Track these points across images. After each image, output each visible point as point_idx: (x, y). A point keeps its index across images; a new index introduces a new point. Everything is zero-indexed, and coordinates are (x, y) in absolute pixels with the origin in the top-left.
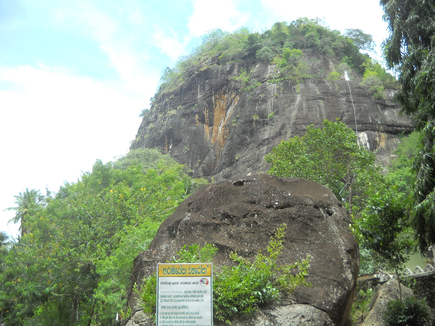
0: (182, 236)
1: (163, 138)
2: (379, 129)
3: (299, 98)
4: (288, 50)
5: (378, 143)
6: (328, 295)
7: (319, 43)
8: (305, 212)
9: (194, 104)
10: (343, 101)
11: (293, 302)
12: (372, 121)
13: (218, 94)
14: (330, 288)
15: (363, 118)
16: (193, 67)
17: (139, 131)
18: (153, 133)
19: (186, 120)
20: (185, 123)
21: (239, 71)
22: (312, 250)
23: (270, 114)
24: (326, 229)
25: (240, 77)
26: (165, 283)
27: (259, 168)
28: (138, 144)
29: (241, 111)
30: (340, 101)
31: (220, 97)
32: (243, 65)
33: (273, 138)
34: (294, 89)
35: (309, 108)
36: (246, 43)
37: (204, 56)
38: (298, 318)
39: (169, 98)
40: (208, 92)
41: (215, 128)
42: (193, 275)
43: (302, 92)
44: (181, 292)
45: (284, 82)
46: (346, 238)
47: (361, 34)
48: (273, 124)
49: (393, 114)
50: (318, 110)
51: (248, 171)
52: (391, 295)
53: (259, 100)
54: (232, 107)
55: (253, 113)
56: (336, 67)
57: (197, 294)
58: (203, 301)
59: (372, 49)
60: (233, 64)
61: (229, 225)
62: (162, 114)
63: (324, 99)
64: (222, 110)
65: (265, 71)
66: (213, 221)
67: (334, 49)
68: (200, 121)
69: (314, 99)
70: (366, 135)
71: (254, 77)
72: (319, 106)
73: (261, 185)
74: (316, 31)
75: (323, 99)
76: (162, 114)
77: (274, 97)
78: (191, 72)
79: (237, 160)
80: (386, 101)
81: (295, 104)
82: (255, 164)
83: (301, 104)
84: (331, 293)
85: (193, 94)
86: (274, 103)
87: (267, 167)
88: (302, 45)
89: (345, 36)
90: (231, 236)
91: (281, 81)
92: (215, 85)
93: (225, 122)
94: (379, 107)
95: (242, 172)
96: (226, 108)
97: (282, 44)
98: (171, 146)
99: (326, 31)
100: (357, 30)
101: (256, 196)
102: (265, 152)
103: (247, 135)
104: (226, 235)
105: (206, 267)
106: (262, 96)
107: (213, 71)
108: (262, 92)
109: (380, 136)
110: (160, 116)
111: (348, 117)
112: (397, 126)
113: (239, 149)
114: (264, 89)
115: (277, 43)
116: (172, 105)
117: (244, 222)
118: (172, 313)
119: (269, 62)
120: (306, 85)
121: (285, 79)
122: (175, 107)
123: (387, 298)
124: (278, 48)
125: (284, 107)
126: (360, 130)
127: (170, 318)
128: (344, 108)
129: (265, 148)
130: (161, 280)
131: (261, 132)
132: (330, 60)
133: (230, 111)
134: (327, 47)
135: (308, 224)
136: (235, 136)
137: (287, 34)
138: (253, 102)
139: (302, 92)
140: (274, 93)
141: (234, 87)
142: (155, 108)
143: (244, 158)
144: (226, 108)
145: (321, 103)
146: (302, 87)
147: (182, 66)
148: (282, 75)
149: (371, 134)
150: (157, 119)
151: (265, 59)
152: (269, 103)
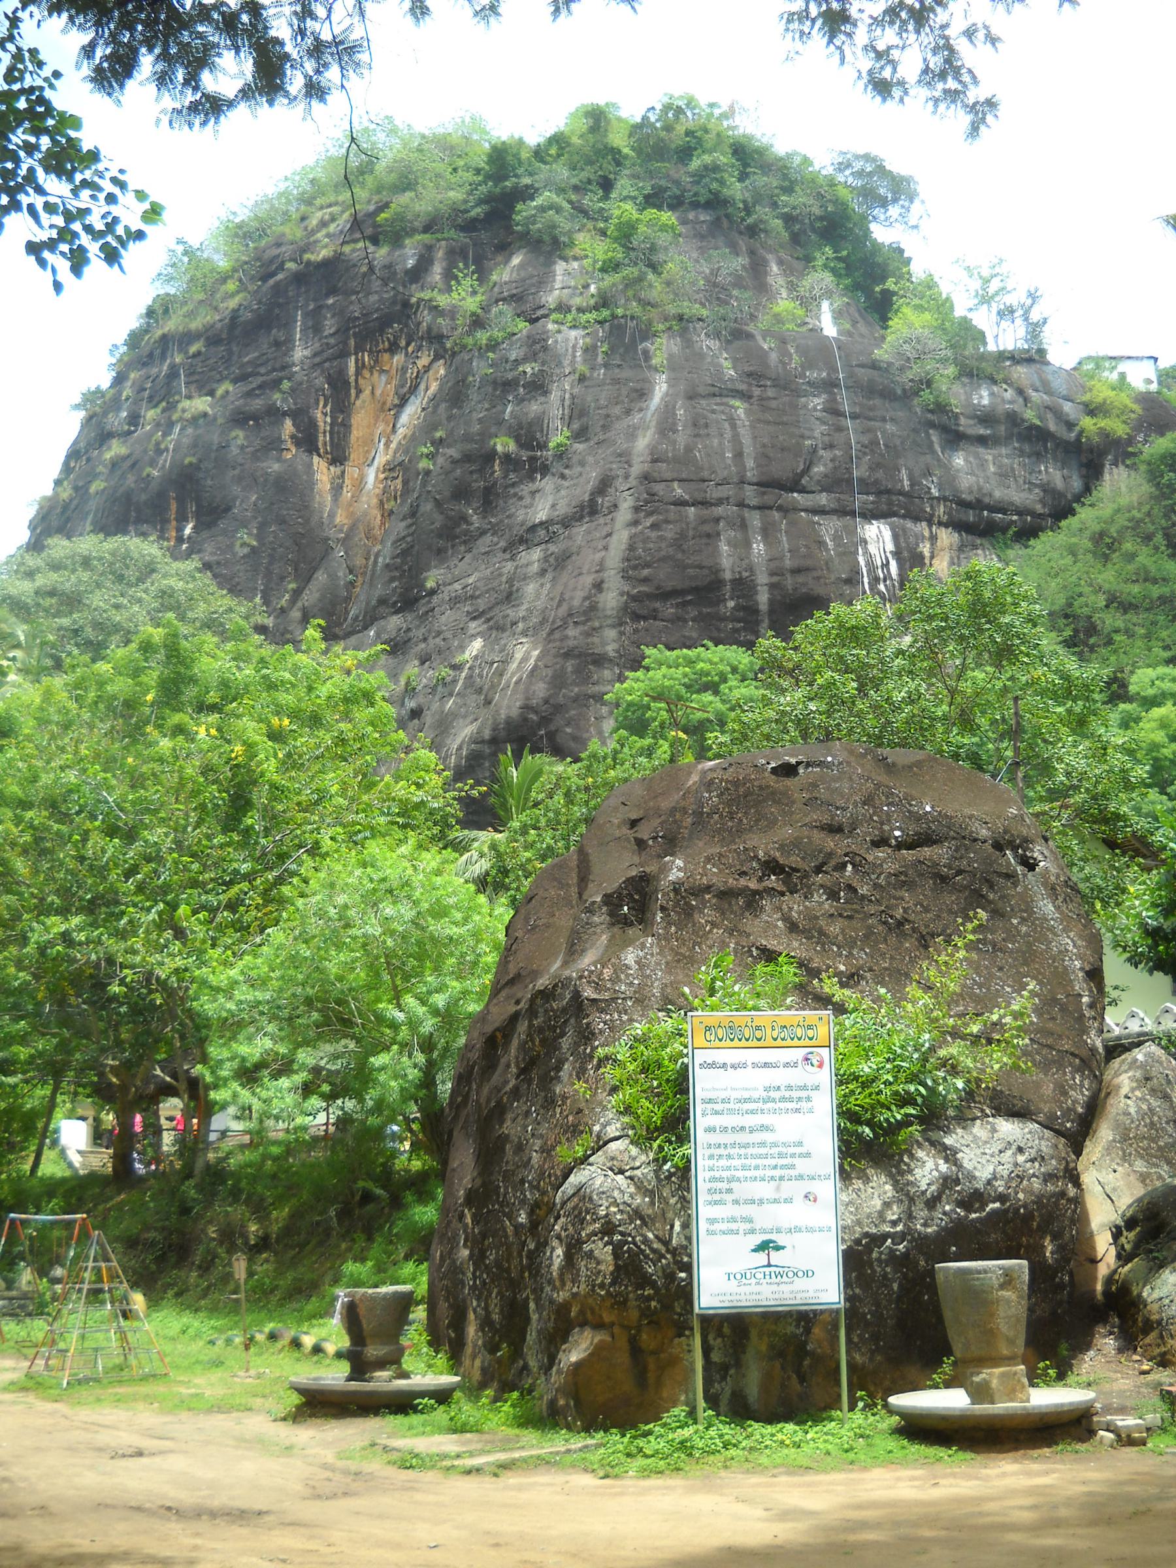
0: (670, 924)
1: (161, 495)
2: (932, 515)
3: (660, 388)
4: (629, 210)
5: (927, 561)
6: (1065, 1093)
7: (739, 196)
8: (973, 860)
9: (276, 384)
10: (815, 409)
11: (988, 1111)
12: (912, 485)
13: (371, 352)
14: (1065, 1073)
15: (880, 474)
16: (278, 245)
17: (66, 464)
18: (123, 477)
19: (246, 437)
20: (242, 447)
21: (449, 276)
22: (1001, 969)
23: (558, 439)
24: (1029, 910)
25: (454, 295)
26: (712, 1065)
27: (514, 624)
28: (63, 513)
29: (450, 418)
30: (805, 406)
31: (376, 361)
32: (462, 253)
33: (567, 522)
34: (646, 353)
35: (698, 425)
36: (478, 171)
37: (322, 208)
38: (1009, 1153)
39: (186, 352)
40: (332, 341)
41: (352, 471)
42: (784, 1043)
43: (673, 366)
44: (756, 1089)
45: (611, 326)
46: (1081, 937)
47: (881, 170)
48: (567, 472)
49: (983, 465)
50: (728, 434)
51: (472, 632)
52: (1153, 1091)
53: (517, 384)
54: (418, 402)
55: (493, 430)
56: (792, 287)
57: (795, 1094)
58: (811, 1111)
59: (916, 227)
60: (429, 248)
61: (782, 894)
62: (158, 410)
63: (750, 397)
64: (382, 410)
65: (544, 280)
66: (743, 882)
67: (789, 219)
68: (298, 443)
69: (714, 395)
70: (887, 534)
71: (504, 300)
72: (732, 421)
73: (851, 779)
74: (729, 151)
75: (745, 396)
76: (158, 410)
77: (572, 377)
78: (271, 261)
79: (432, 592)
80: (963, 421)
81: (647, 408)
82: (496, 610)
83: (668, 410)
84: (1071, 1087)
85: (277, 344)
86: (573, 397)
87: (542, 623)
88: (677, 197)
89: (824, 172)
90: (793, 927)
91: (600, 322)
92: (358, 318)
93: (391, 452)
94: (935, 436)
95: (448, 635)
96: (396, 401)
97: (607, 185)
98: (190, 525)
99: (761, 152)
100: (867, 157)
101: (844, 809)
102: (535, 567)
103: (468, 503)
104: (780, 923)
105: (815, 1021)
106: (529, 370)
107: (355, 266)
108: (532, 357)
109: (933, 538)
110: (151, 414)
111: (831, 465)
112: (993, 509)
113: (440, 552)
114: (537, 347)
115: (589, 182)
116: (196, 377)
117: (822, 886)
118: (733, 1145)
119: (559, 248)
120: (688, 343)
121: (614, 316)
122: (208, 388)
123: (1142, 1099)
124: (590, 201)
125: (608, 416)
126: (871, 515)
127: (729, 1157)
128: (817, 434)
129: (536, 554)
130: (701, 1056)
131: (521, 498)
132: (770, 257)
133: (411, 414)
134: (762, 212)
135: (983, 896)
136: (427, 507)
137: (626, 150)
138: (495, 389)
139: (673, 366)
140: (573, 362)
141: (429, 329)
142: (129, 383)
143: (457, 586)
144: (396, 401)
145: (740, 408)
146: (675, 349)
147: (236, 235)
148: (604, 301)
149: (904, 530)
150: (136, 425)
151: (546, 238)
152: (554, 396)
